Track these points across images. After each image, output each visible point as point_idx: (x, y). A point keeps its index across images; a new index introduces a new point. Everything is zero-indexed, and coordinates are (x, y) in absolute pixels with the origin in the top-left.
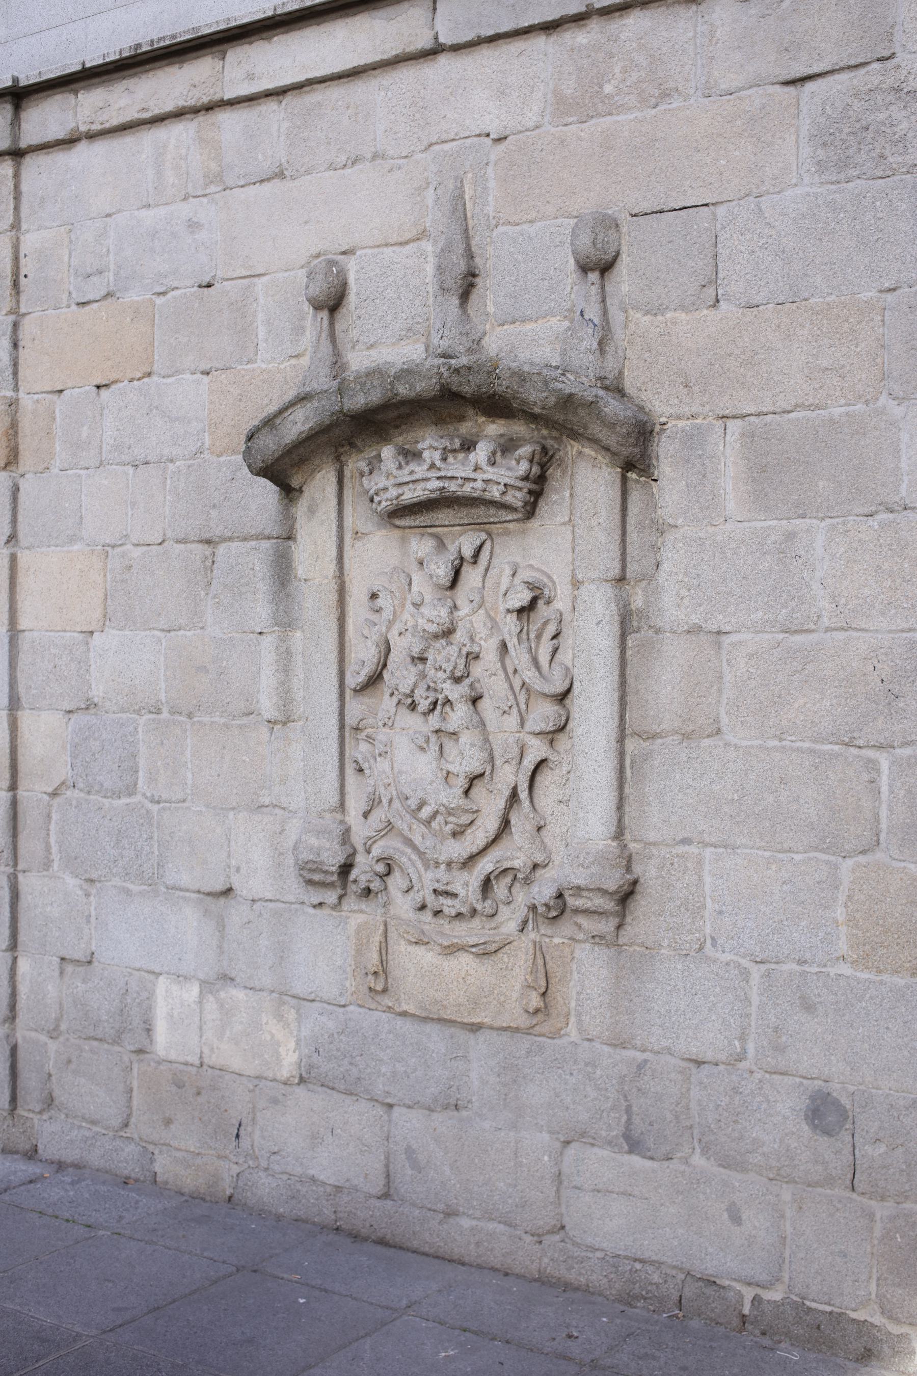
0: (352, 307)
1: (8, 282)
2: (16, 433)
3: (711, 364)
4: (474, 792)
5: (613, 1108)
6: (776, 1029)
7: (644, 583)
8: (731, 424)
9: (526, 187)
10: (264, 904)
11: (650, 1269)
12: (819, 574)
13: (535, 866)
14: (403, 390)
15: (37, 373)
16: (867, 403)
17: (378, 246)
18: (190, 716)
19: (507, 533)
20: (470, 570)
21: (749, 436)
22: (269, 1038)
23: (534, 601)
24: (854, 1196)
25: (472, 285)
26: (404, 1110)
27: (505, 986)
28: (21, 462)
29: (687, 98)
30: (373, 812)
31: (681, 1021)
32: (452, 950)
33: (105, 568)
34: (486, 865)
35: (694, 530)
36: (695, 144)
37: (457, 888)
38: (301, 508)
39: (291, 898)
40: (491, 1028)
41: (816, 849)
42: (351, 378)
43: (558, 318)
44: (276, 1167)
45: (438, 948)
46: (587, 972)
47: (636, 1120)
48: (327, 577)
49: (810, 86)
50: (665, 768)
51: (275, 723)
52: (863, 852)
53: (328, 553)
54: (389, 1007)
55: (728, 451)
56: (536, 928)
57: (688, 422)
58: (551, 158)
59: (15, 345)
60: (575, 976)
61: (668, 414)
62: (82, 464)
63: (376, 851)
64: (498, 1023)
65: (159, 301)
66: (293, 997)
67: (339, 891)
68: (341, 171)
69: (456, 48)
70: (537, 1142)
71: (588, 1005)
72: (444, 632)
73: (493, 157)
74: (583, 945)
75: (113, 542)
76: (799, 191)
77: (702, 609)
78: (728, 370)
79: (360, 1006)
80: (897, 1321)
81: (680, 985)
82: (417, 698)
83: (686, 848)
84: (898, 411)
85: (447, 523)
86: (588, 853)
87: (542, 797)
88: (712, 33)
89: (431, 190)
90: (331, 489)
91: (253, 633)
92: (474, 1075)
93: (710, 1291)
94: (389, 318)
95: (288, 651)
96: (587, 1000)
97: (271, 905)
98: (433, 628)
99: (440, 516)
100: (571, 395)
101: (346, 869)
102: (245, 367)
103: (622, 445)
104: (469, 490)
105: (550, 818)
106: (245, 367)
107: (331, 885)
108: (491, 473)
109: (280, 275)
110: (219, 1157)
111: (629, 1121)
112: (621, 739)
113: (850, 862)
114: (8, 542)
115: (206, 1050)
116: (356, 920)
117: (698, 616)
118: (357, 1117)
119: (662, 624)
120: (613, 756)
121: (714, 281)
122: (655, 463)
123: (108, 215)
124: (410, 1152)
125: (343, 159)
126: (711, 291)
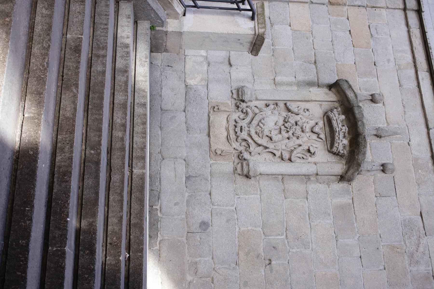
0: (372, 105)
1: (374, 5)
2: (338, 5)
4: (267, 138)
5: (196, 173)
6: (221, 213)
8: (351, 200)
11: (159, 182)
12: (322, 221)
13: (250, 153)
14: (360, 123)
15: (353, 12)
16: (358, 232)
18: (273, 55)
19: (325, 145)
21: (349, 205)
22: (196, 76)
23: (311, 153)
24: (186, 233)
25: (378, 137)
26: (185, 115)
27: (220, 144)
28: (330, 6)
29: (418, 190)
32: (227, 129)
33: (307, 31)
34: (250, 141)
37: (243, 133)
38: (326, 90)
40: (210, 140)
41: (263, 222)
44: (162, 77)
45: (227, 126)
47: (194, 179)
49: (420, 218)
52: (264, 233)
54: (210, 112)
55: (346, 200)
56: (236, 153)
59: (359, 6)
60: (225, 163)
62: (331, 25)
63: (249, 110)
64: (211, 142)
65: (371, 50)
66: (207, 84)
67: (237, 99)
69: (428, 134)
70: (184, 153)
73: (405, 142)
75: (313, 34)
76: (400, 216)
79: (208, 103)
80: (160, 244)
81: (228, 190)
82: (288, 123)
84: (356, 239)
88: (431, 196)
89: (398, 126)
90: (332, 99)
92: (196, 135)
93: (157, 198)
95: (292, 85)
98: (304, 128)
100: (360, 166)
101: (243, 101)
107: (238, 97)
108: (341, 144)
109: (378, 85)
110: (162, 60)
111: (194, 177)
112: (282, 175)
113: (261, 230)
114: (311, 1)
115: (189, 57)
116: (229, 102)
118: (180, 103)
120: (279, 173)
121: (381, 196)
123: (390, 36)
124: (174, 117)
125: (404, 103)
126: (378, 195)
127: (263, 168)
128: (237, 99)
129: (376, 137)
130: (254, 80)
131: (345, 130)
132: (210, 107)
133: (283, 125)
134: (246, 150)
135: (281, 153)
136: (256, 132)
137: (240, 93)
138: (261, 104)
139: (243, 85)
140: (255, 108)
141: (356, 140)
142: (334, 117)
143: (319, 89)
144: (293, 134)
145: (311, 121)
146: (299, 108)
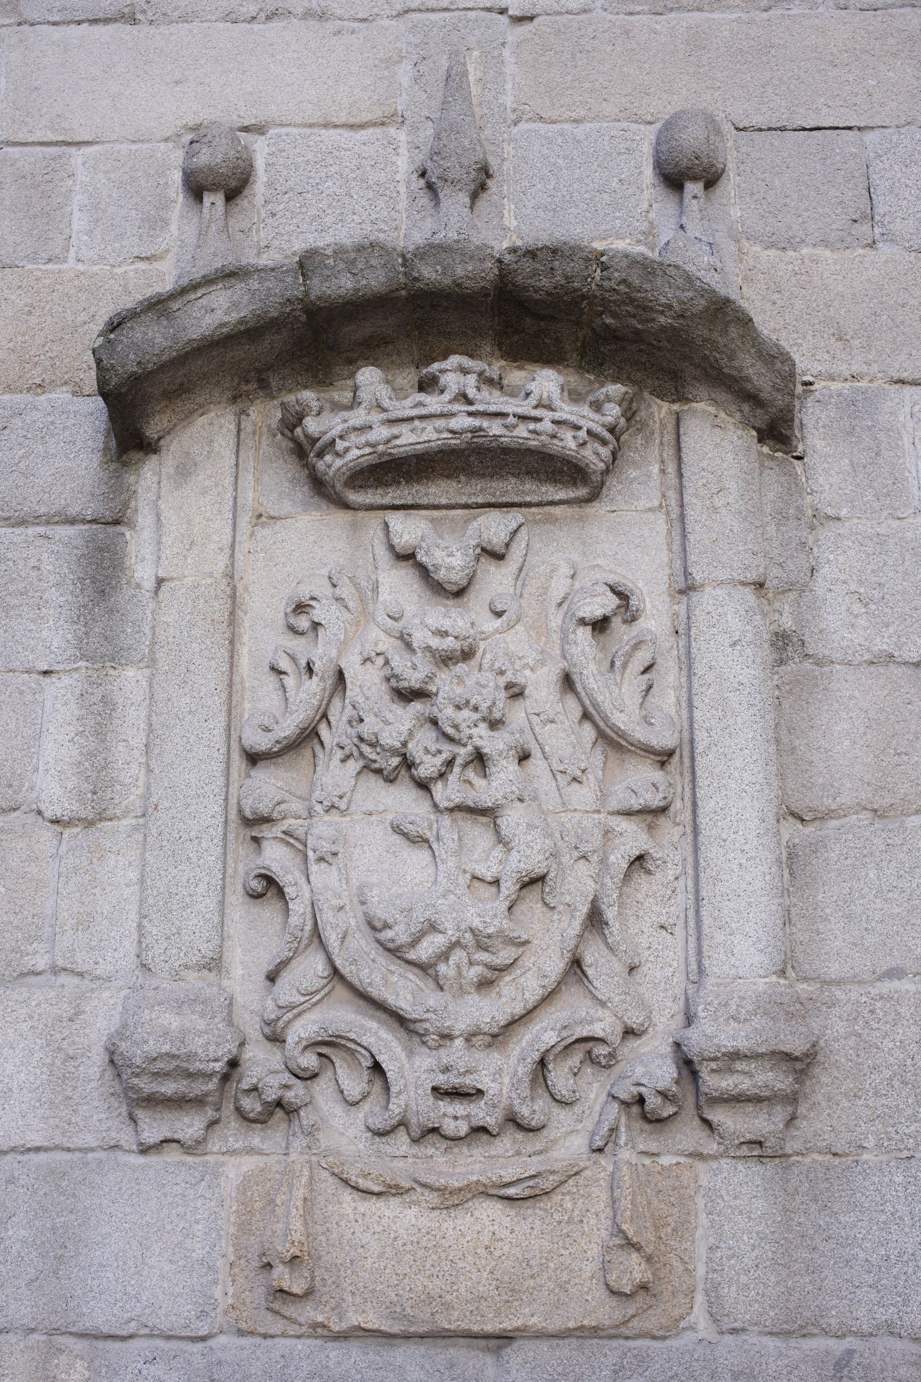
0: (259, 200)
3: (875, 314)
7: (792, 596)
9: (569, 78)
10: (19, 1158)
13: (629, 1033)
14: (429, 273)
17: (312, 126)
19: (552, 520)
20: (492, 569)
25: (483, 187)
30: (294, 963)
31: (910, 1271)
32: (452, 1198)
34: (544, 1033)
35: (869, 524)
36: (830, 58)
37: (484, 1081)
38: (149, 476)
39: (91, 1140)
40: (540, 1335)
42: (329, 252)
43: (628, 241)
45: (434, 1198)
46: (728, 1209)
48: (211, 575)
50: (849, 861)
51: (68, 824)
53: (216, 538)
54: (315, 1326)
57: (847, 385)
58: (609, 48)
60: (703, 1219)
61: (815, 372)
63: (303, 1029)
66: (82, 1335)
68: (245, 25)
71: (731, 1267)
72: (463, 651)
73: (510, 38)
74: (714, 1164)
77: (891, 630)
78: (902, 323)
79: (241, 1333)
81: (902, 1210)
83: (896, 984)
85: (444, 501)
86: (742, 998)
87: (632, 919)
91: (28, 672)
94: (329, 220)
96: (729, 1258)
97: (42, 1157)
98: (449, 643)
99: (433, 490)
102: (42, 267)
103: (778, 390)
104: (525, 434)
105: (647, 953)
106: (42, 267)
107: (199, 1102)
109: (124, 148)
116: (235, 1170)
117: (886, 640)
119: (827, 652)
122: (799, 436)
125: (253, 9)
127: (743, 953)
128: (210, 1113)
129: (484, 196)
130: (56, 970)
131: (465, 371)
132: (277, 1326)
133: (423, 785)
134: (606, 1064)
135: (628, 813)
136: (484, 984)
137: (168, 1088)
138: (254, 939)
139: (98, 1057)
140: (285, 979)
141: (538, 312)
142: (372, 436)
143: (144, 519)
144: (494, 724)
145: (385, 595)
146: (284, 664)
